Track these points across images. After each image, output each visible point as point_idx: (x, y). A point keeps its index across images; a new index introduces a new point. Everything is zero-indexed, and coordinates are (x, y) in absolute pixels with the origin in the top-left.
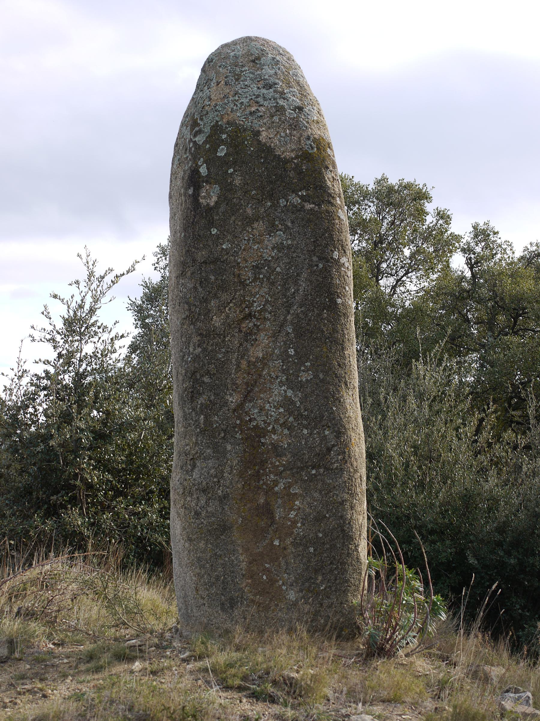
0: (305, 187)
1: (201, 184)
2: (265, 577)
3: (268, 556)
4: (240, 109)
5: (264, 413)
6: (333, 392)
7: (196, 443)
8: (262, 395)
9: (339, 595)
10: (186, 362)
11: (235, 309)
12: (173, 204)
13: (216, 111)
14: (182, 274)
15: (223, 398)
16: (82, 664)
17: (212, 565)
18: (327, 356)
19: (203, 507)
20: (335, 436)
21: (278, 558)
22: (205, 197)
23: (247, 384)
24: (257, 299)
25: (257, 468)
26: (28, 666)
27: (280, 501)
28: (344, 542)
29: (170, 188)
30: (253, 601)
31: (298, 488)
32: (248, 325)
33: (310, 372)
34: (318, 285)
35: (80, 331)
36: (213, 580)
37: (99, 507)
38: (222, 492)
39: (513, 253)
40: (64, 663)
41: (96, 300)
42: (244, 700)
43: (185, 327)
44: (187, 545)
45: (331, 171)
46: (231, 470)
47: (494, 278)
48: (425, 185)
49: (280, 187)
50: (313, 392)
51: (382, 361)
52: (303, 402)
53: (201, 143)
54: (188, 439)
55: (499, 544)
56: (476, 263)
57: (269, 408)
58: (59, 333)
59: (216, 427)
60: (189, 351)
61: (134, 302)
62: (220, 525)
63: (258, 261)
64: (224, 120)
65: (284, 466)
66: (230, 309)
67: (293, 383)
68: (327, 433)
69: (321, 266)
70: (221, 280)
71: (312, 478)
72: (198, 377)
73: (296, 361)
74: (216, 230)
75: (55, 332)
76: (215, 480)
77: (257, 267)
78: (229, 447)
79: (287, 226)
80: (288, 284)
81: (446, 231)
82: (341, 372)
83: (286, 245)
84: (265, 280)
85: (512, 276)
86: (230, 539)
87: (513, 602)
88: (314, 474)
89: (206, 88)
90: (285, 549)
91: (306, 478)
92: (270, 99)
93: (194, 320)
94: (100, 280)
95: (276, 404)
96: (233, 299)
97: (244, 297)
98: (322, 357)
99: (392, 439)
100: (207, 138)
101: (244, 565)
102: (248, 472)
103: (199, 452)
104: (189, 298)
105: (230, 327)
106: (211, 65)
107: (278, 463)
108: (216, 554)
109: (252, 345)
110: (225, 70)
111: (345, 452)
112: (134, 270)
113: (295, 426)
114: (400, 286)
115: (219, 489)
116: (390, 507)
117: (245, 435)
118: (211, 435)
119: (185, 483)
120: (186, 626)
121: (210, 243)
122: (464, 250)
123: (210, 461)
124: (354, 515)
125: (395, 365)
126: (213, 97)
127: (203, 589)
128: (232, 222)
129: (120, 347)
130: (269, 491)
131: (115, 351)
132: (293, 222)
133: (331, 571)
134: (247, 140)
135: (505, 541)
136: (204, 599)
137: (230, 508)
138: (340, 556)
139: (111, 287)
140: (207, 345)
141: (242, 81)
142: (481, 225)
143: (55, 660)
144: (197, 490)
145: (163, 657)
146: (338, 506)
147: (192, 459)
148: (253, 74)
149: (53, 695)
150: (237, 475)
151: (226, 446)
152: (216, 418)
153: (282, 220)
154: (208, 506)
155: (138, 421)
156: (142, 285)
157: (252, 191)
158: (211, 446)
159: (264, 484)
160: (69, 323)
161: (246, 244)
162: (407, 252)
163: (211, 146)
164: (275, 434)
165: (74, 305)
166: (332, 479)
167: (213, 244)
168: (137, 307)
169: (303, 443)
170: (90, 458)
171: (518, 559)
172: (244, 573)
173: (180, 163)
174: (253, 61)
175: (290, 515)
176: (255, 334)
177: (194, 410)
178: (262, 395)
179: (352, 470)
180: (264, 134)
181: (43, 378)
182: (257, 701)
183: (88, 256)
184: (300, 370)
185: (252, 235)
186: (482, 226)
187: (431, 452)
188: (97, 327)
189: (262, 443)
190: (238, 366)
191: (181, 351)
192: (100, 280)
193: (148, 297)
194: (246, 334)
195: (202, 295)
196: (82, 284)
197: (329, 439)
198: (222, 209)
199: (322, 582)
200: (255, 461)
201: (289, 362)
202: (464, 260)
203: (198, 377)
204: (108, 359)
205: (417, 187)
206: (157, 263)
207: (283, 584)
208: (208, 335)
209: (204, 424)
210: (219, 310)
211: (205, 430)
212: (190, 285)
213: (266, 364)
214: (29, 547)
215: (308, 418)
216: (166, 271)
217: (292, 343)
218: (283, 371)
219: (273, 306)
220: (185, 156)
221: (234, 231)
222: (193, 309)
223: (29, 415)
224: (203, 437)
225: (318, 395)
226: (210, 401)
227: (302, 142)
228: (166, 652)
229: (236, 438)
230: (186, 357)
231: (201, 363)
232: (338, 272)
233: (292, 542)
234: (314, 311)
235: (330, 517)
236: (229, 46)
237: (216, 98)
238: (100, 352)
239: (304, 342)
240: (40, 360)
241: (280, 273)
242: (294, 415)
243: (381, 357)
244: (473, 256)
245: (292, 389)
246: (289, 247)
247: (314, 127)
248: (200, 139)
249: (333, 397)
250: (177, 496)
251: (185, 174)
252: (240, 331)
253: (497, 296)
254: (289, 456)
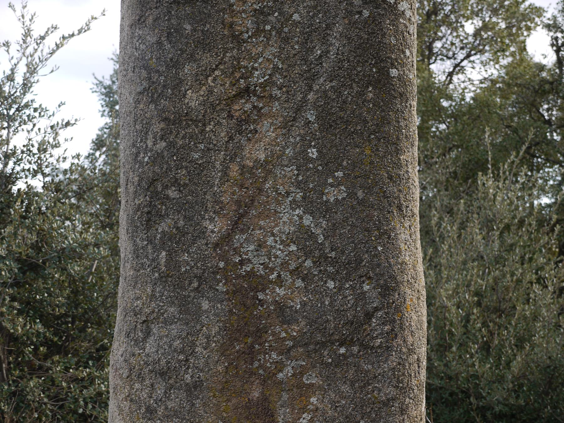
5: (264, 250)
6: (379, 221)
8: (262, 223)
10: (141, 163)
11: (222, 80)
14: (139, 20)
15: (198, 224)
18: (372, 163)
19: (160, 400)
20: (380, 293)
23: (238, 203)
24: (260, 64)
25: (250, 340)
27: (285, 396)
31: (316, 376)
32: (243, 106)
33: (343, 188)
34: (360, 45)
37: (26, 369)
38: (192, 377)
41: (32, 70)
43: (142, 106)
46: (208, 343)
50: (346, 220)
51: (433, 172)
52: (329, 236)
54: (140, 289)
57: (273, 244)
59: (186, 271)
60: (147, 146)
61: (101, 82)
65: (294, 339)
66: (214, 80)
67: (313, 204)
68: (366, 287)
69: (366, 13)
70: (202, 31)
71: (339, 361)
72: (160, 189)
73: (320, 168)
76: (182, 357)
77: (261, 12)
78: (205, 305)
80: (312, 42)
82: (392, 189)
84: (274, 33)
88: (343, 355)
91: (330, 360)
93: (156, 96)
94: (39, 42)
95: (284, 237)
96: (220, 63)
97: (238, 60)
98: (362, 164)
99: (446, 282)
102: (235, 347)
103: (156, 310)
104: (150, 59)
105: (214, 109)
109: (249, 140)
111: (394, 321)
112: (89, 29)
113: (315, 275)
114: (457, 74)
116: (442, 378)
117: (231, 287)
122: (548, 27)
123: (173, 327)
125: (451, 180)
129: (66, 140)
130: (268, 379)
131: (57, 146)
137: (204, 405)
140: (176, 137)
144: (151, 371)
146: (380, 408)
147: (144, 321)
150: (217, 351)
151: (200, 304)
152: (186, 257)
154: (168, 398)
156: (112, 59)
158: (176, 302)
159: (260, 366)
162: (469, 27)
164: (280, 287)
168: (105, 88)
169: (327, 303)
170: (13, 299)
175: (301, 420)
176: (255, 121)
177: (150, 242)
178: (262, 223)
179: (404, 350)
183: (24, 7)
184: (326, 184)
187: (500, 302)
188: (32, 110)
189: (260, 300)
191: (134, 145)
192: (39, 42)
194: (240, 122)
196: (14, 48)
197: (370, 298)
200: (246, 331)
201: (308, 169)
202: (548, 40)
203: (160, 189)
204: (48, 156)
208: (177, 122)
209: (165, 266)
210: (196, 81)
212: (152, 39)
213: (270, 172)
215: (337, 262)
217: (314, 139)
218: (298, 184)
219: (286, 77)
222: (155, 77)
224: (164, 287)
225: (353, 226)
226: (178, 228)
229: (217, 290)
230: (142, 155)
232: (393, 25)
234: (351, 88)
238: (36, 146)
239: (334, 138)
241: (299, 22)
242: (314, 257)
243: (433, 167)
245: (311, 214)
250: (119, 381)
254: (303, 323)
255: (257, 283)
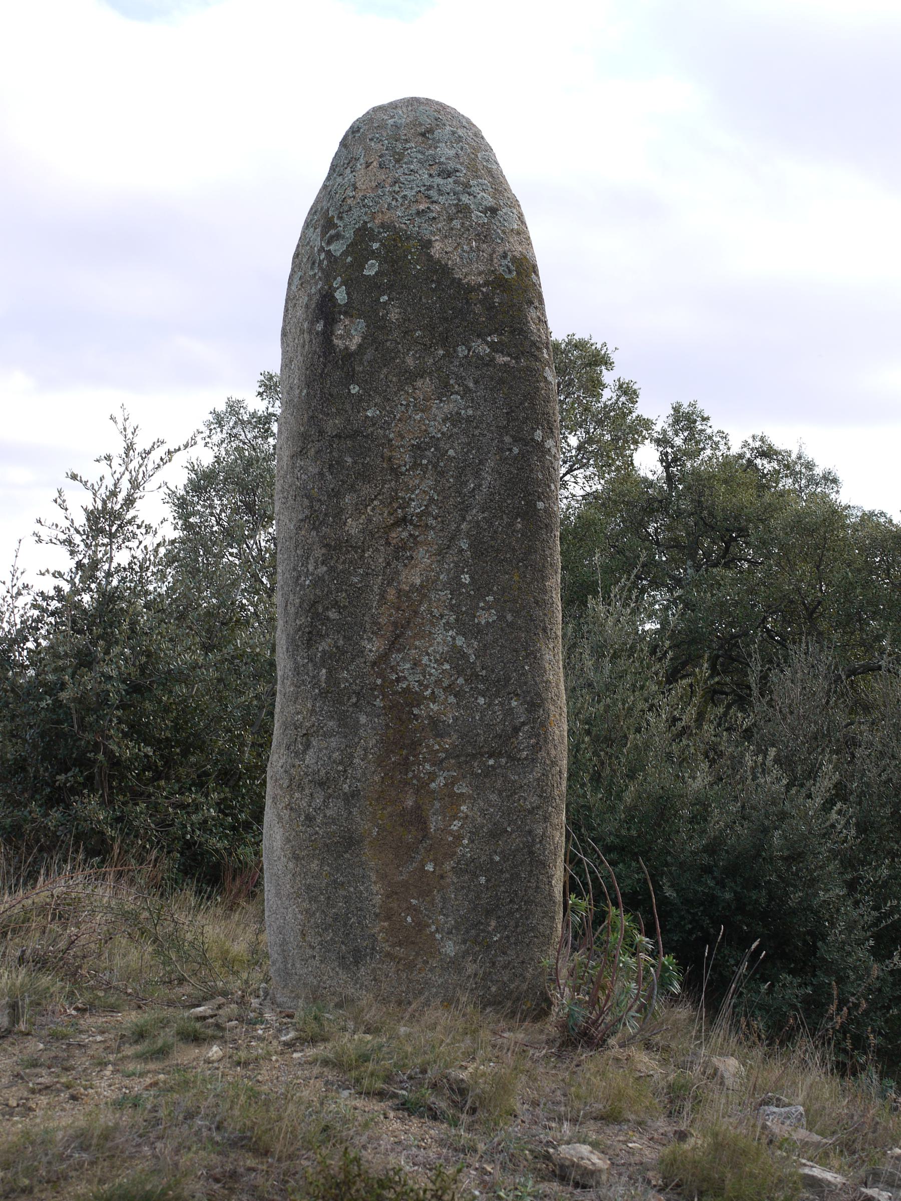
0: (496, 330)
1: (337, 316)
2: (409, 919)
3: (416, 887)
4: (402, 205)
5: (419, 669)
7: (313, 711)
8: (417, 643)
9: (521, 950)
10: (302, 586)
11: (381, 510)
12: (288, 345)
13: (364, 206)
16: (127, 1045)
17: (329, 898)
18: (520, 588)
21: (431, 891)
22: (341, 337)
23: (395, 624)
24: (417, 495)
26: (41, 1046)
27: (437, 805)
28: (532, 871)
29: (284, 321)
30: (388, 954)
32: (400, 534)
33: (493, 611)
35: (110, 530)
36: (329, 920)
38: (350, 787)
39: (729, 449)
40: (96, 1042)
41: (135, 485)
42: (392, 1114)
43: (303, 532)
44: (291, 865)
45: (536, 308)
46: (365, 755)
47: (699, 483)
48: (605, 344)
49: (458, 327)
50: (496, 641)
53: (338, 254)
55: (707, 870)
56: (675, 460)
58: (78, 532)
59: (345, 688)
61: (174, 492)
62: (343, 837)
63: (420, 438)
64: (376, 221)
65: (446, 751)
66: (373, 509)
68: (514, 704)
69: (516, 450)
70: (362, 464)
71: (488, 772)
72: (320, 610)
73: (472, 592)
74: (357, 388)
75: (72, 530)
76: (340, 768)
77: (418, 447)
78: (363, 719)
79: (467, 387)
80: (465, 476)
81: (631, 412)
83: (465, 416)
84: (430, 467)
85: (726, 482)
86: (358, 859)
87: (725, 956)
88: (492, 766)
89: (348, 171)
90: (442, 877)
91: (480, 771)
92: (448, 194)
95: (438, 657)
96: (379, 494)
98: (511, 589)
100: (348, 246)
101: (378, 900)
106: (357, 137)
107: (437, 747)
108: (335, 881)
110: (379, 146)
112: (195, 443)
115: (344, 782)
118: (335, 701)
119: (293, 771)
120: (283, 988)
121: (348, 407)
122: (658, 442)
123: (332, 739)
124: (549, 830)
126: (358, 184)
127: (313, 933)
128: (382, 376)
130: (422, 788)
132: (476, 382)
133: (511, 913)
134: (411, 253)
135: (716, 865)
136: (314, 948)
137: (361, 813)
138: (526, 891)
139: (159, 466)
140: (337, 562)
141: (406, 163)
142: (685, 406)
143: (83, 1037)
144: (310, 782)
145: (253, 1037)
147: (305, 734)
148: (424, 154)
149: (87, 1096)
152: (345, 674)
153: (460, 379)
155: (194, 668)
156: (187, 467)
157: (416, 331)
159: (414, 777)
160: (93, 517)
161: (403, 412)
163: (355, 259)
164: (434, 703)
165: (103, 493)
166: (519, 775)
167: (352, 409)
168: (178, 499)
169: (477, 718)
171: (735, 892)
172: (378, 911)
173: (301, 285)
174: (423, 135)
177: (311, 660)
178: (417, 643)
179: (548, 762)
180: (438, 246)
181: (52, 598)
182: (409, 1116)
184: (477, 607)
185: (414, 398)
186: (685, 408)
188: (135, 526)
189: (415, 715)
190: (383, 596)
191: (294, 569)
193: (195, 486)
194: (397, 549)
195: (332, 486)
196: (116, 461)
197: (517, 713)
198: (368, 357)
199: (496, 930)
200: (403, 741)
201: (461, 594)
203: (320, 610)
205: (593, 347)
206: (209, 437)
207: (437, 930)
211: (328, 692)
212: (313, 470)
213: (425, 595)
214: (33, 853)
215: (487, 680)
216: (222, 449)
218: (452, 608)
219: (441, 508)
220: (311, 273)
221: (386, 391)
222: (317, 506)
223: (25, 651)
224: (324, 702)
225: (502, 646)
226: (337, 647)
227: (495, 261)
228: (256, 1030)
229: (375, 705)
231: (326, 589)
233: (453, 868)
235: (513, 831)
236: (386, 110)
237: (364, 187)
240: (48, 571)
241: (454, 458)
242: (466, 675)
244: (669, 450)
245: (464, 635)
246: (469, 420)
247: (513, 239)
248: (337, 248)
249: (526, 650)
251: (310, 299)
252: (388, 543)
253: (702, 509)
254: (455, 736)
255: (413, 699)
